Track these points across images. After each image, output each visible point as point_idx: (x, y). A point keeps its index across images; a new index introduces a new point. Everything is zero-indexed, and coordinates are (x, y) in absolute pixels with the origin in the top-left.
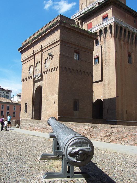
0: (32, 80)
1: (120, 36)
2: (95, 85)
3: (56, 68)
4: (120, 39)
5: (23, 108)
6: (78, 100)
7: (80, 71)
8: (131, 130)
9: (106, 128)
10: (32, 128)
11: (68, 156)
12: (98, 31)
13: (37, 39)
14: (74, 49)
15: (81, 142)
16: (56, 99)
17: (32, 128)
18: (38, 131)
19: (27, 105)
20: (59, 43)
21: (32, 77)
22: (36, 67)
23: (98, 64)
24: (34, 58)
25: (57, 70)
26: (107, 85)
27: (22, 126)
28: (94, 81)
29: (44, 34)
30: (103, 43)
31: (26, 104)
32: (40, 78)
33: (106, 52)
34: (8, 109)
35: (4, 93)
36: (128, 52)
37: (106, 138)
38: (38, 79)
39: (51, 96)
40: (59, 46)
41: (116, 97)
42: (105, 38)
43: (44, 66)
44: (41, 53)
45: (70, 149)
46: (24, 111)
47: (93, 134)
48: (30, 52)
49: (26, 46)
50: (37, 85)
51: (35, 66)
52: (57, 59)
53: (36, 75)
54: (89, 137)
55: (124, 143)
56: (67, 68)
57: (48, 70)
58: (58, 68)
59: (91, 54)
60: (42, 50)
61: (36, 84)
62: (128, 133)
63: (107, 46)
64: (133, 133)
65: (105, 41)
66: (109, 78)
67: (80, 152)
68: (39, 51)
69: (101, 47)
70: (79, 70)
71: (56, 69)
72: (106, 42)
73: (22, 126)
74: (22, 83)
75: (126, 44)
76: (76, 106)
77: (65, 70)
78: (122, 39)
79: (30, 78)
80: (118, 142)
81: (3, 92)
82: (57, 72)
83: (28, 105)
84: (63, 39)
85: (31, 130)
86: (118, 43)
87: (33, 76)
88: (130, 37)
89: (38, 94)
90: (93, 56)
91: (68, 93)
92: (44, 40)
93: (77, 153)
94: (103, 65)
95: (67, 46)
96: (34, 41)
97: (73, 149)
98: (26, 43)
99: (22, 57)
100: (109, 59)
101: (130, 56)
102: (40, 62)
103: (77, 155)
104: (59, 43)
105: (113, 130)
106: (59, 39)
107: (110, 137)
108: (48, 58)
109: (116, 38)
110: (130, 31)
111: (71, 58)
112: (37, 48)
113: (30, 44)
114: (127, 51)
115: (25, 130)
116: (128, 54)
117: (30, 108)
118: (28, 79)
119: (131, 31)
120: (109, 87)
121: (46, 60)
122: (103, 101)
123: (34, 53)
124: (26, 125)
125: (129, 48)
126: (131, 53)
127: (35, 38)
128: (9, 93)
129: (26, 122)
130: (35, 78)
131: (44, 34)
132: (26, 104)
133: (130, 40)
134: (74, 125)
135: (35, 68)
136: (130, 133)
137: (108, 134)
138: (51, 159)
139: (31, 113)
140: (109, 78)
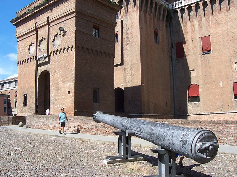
0: (34, 62)
1: (145, 8)
3: (71, 47)
4: (145, 12)
5: (20, 99)
6: (99, 89)
7: (101, 52)
10: (45, 127)
11: (198, 152)
13: (41, 8)
14: (93, 24)
15: (209, 136)
16: (72, 87)
18: (56, 129)
20: (74, 15)
22: (39, 45)
23: (117, 44)
24: (37, 33)
25: (71, 51)
26: (129, 70)
27: (29, 124)
29: (52, 2)
31: (24, 95)
32: (46, 60)
33: (127, 28)
36: (155, 29)
38: (44, 61)
40: (75, 18)
41: (141, 84)
42: (127, 10)
44: (47, 27)
45: (198, 145)
46: (23, 104)
48: (31, 25)
49: (25, 17)
51: (38, 44)
52: (72, 36)
53: (41, 56)
56: (85, 48)
58: (74, 48)
59: (111, 30)
60: (48, 24)
61: (39, 68)
65: (126, 14)
66: (132, 61)
67: (211, 147)
68: (44, 24)
70: (98, 51)
72: (128, 16)
73: (29, 124)
74: (18, 67)
75: (152, 19)
76: (96, 97)
77: (81, 50)
78: (148, 12)
79: (30, 61)
82: (72, 54)
84: (79, 10)
85: (45, 129)
88: (158, 10)
89: (43, 82)
91: (86, 80)
92: (52, 10)
93: (207, 148)
94: (124, 44)
95: (85, 19)
96: (36, 11)
97: (203, 144)
98: (24, 12)
99: (18, 32)
100: (132, 37)
101: (156, 34)
102: (47, 39)
103: (208, 151)
104: (75, 15)
106: (74, 10)
108: (57, 34)
109: (141, 11)
110: (157, 3)
111: (90, 34)
112: (41, 19)
113: (30, 14)
114: (153, 28)
115: (35, 129)
116: (154, 31)
117: (31, 100)
119: (158, 2)
120: (131, 73)
121: (55, 36)
122: (123, 89)
123: (36, 26)
124: (36, 123)
125: (156, 24)
126: (158, 31)
127: (38, 7)
129: (36, 118)
130: (39, 60)
131: (52, 2)
132: (24, 95)
133: (157, 13)
135: (38, 47)
138: (120, 162)
139: (33, 106)
140: (132, 61)
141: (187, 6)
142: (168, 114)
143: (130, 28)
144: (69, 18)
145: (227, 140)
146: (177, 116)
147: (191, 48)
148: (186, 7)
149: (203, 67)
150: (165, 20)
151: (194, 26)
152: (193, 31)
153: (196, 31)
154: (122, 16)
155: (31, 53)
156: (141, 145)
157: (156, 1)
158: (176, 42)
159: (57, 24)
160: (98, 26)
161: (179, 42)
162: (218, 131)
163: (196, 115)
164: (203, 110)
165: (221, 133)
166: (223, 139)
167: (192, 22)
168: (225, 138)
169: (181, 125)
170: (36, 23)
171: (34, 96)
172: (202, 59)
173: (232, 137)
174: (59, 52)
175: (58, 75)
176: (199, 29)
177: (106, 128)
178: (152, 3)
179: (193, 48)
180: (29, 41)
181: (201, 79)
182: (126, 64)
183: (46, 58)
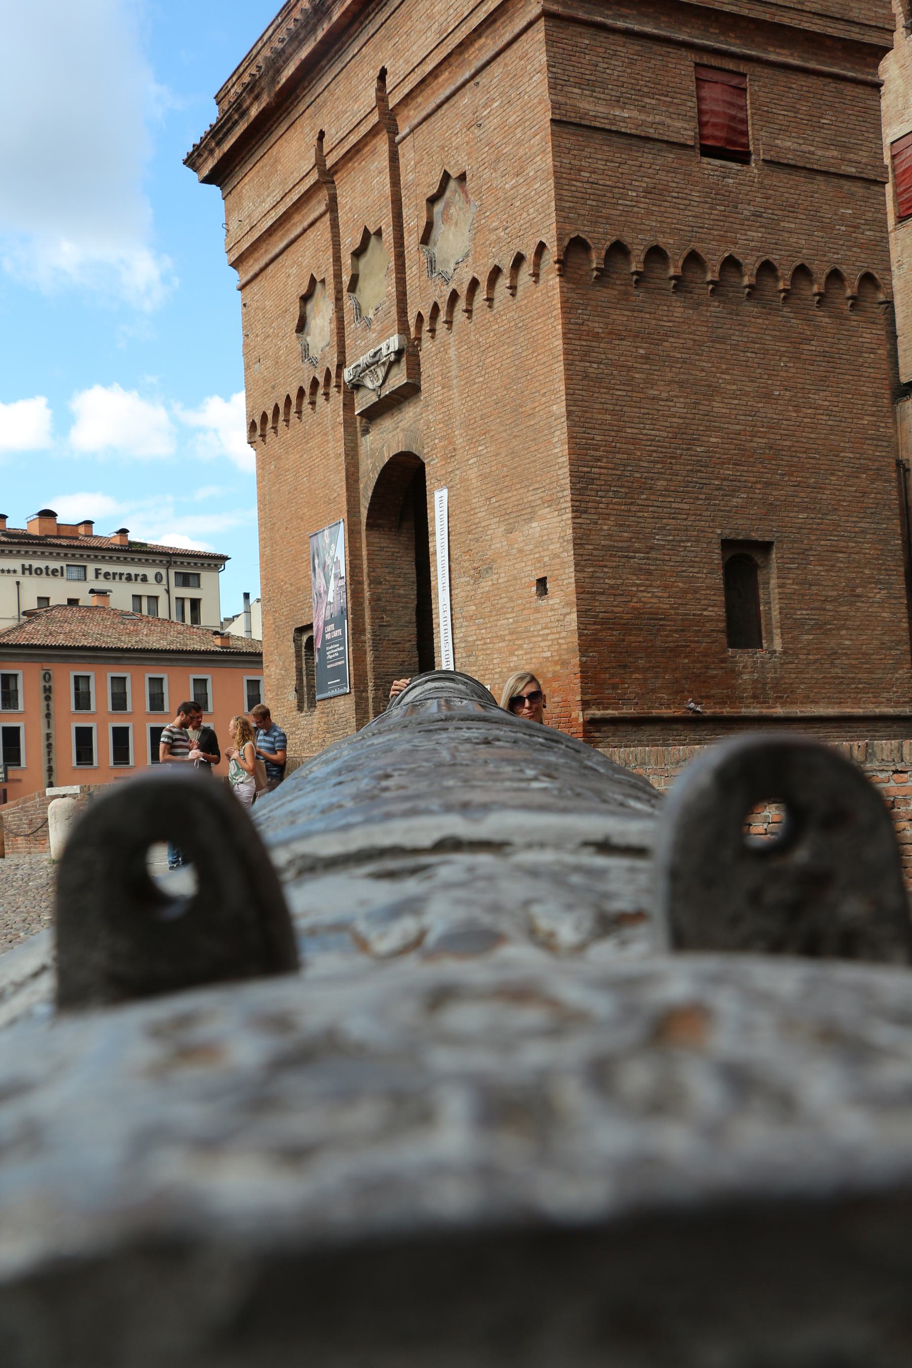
3: (529, 254)
16: (555, 547)
19: (311, 639)
21: (333, 390)
22: (353, 285)
24: (333, 207)
32: (399, 378)
35: (158, 578)
39: (510, 531)
43: (424, 259)
46: (292, 697)
49: (254, 112)
51: (346, 279)
53: (364, 359)
57: (463, 291)
81: (150, 572)
87: (339, 375)
90: (887, 141)
121: (432, 201)
128: (205, 576)
132: (301, 630)
135: (348, 303)
144: (508, 37)
155: (314, 352)
159: (439, 106)
175: (473, 474)
180: (294, 270)
183: (397, 361)
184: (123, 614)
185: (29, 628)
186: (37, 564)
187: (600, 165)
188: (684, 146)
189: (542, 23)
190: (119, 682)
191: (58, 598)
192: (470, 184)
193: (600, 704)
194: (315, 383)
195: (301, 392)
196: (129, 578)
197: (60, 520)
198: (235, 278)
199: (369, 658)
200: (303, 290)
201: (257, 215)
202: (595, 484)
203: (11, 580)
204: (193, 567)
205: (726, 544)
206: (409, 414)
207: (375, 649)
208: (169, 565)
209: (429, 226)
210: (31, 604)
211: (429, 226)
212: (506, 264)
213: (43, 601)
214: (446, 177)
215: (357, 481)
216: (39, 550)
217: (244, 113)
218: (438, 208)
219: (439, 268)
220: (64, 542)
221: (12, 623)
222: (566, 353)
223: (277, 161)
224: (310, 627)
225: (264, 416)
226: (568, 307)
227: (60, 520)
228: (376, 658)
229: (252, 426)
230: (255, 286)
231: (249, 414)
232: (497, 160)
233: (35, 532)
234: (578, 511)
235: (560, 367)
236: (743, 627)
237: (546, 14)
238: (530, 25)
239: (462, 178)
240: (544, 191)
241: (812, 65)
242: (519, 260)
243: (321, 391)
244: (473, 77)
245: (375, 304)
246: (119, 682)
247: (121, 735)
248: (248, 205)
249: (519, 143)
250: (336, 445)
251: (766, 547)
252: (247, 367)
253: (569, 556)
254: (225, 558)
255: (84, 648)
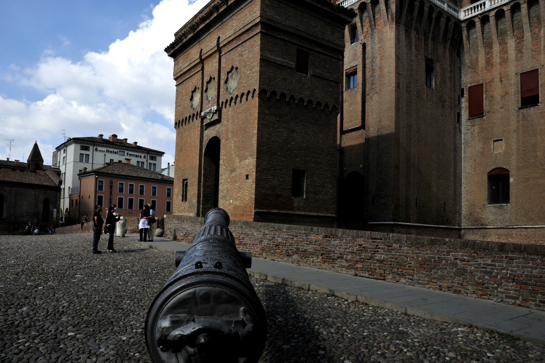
2: (347, 139)
3: (252, 91)
8: (423, 246)
9: (360, 241)
12: (356, 8)
16: (251, 167)
17: (190, 238)
19: (187, 183)
21: (198, 117)
22: (206, 91)
24: (203, 69)
27: (168, 232)
28: (344, 130)
30: (368, 36)
32: (216, 117)
33: (373, 57)
34: (142, 192)
35: (145, 157)
37: (359, 265)
39: (240, 161)
42: (373, 23)
43: (225, 87)
45: (165, 323)
46: (181, 198)
47: (327, 255)
49: (184, 41)
50: (210, 133)
51: (204, 88)
53: (207, 111)
54: (318, 262)
55: (403, 280)
57: (234, 97)
58: (257, 92)
62: (417, 253)
63: (377, 43)
64: (428, 254)
65: (372, 30)
66: (380, 121)
68: (213, 51)
69: (364, 46)
71: (250, 95)
72: (376, 35)
73: (168, 232)
77: (271, 99)
80: (389, 277)
81: (143, 155)
83: (188, 184)
86: (404, 35)
87: (200, 114)
90: (345, 69)
94: (367, 89)
96: (201, 27)
97: (176, 324)
104: (258, 30)
105: (377, 244)
106: (258, 20)
107: (368, 264)
114: (423, 56)
117: (193, 191)
118: (189, 122)
121: (228, 73)
125: (430, 50)
128: (158, 158)
129: (177, 222)
132: (184, 180)
133: (432, 29)
134: (285, 230)
135: (204, 95)
136: (420, 253)
137: (363, 255)
139: (195, 201)
140: (380, 121)
141: (496, 11)
142: (446, 225)
143: (378, 58)
144: (251, 36)
145: (499, 289)
146: (464, 229)
147: (498, 97)
148: (493, 13)
149: (520, 133)
150: (449, 42)
151: (506, 52)
152: (504, 61)
153: (509, 60)
154: (365, 36)
155: (194, 106)
156: (309, 286)
157: (430, 2)
158: (469, 85)
159: (233, 49)
160: (306, 50)
161: (475, 84)
162: (482, 268)
163: (500, 228)
164: (516, 219)
165: (487, 273)
166: (492, 287)
167: (503, 43)
168: (496, 286)
169: (406, 248)
170: (202, 50)
171: (197, 183)
172: (518, 116)
173: (511, 284)
174: (233, 101)
175: (232, 145)
176: (516, 56)
177: (277, 245)
178: (422, 4)
179: (502, 97)
180: (191, 84)
181: (514, 157)
182: (369, 128)
183: (216, 113)
184: (134, 166)
185: (108, 168)
186: (110, 150)
187: (271, 71)
188: (292, 69)
189: (260, 34)
190: (132, 186)
191: (116, 160)
192: (238, 70)
193: (259, 208)
194: (194, 115)
195: (190, 116)
196: (136, 156)
197: (118, 138)
198: (175, 83)
199: (202, 190)
200: (193, 89)
201: (182, 67)
202: (262, 153)
203: (103, 153)
204: (156, 155)
205: (294, 170)
206: (218, 126)
207: (204, 187)
208: (148, 154)
209: (227, 79)
210: (108, 161)
211: (227, 79)
212: (246, 92)
213: (111, 160)
214: (233, 67)
215: (203, 142)
216: (112, 146)
217: (182, 40)
218: (230, 75)
219: (229, 90)
220: (119, 144)
221: (102, 166)
222: (258, 118)
223: (189, 54)
224: (187, 179)
225: (179, 121)
226: (260, 106)
227: (118, 138)
228: (204, 190)
229: (176, 124)
230: (180, 86)
231: (176, 120)
232: (246, 66)
233: (111, 140)
234: (258, 158)
235: (256, 121)
236: (297, 191)
237: (261, 32)
238: (257, 34)
239: (237, 68)
240: (257, 76)
241: (325, 52)
242: (249, 92)
243: (195, 117)
244: (242, 43)
245: (211, 96)
246: (132, 186)
247: (131, 201)
248: (180, 64)
249: (252, 63)
250: (198, 132)
251: (304, 172)
252: (176, 107)
253: (254, 170)
254: (164, 153)
255: (123, 175)
